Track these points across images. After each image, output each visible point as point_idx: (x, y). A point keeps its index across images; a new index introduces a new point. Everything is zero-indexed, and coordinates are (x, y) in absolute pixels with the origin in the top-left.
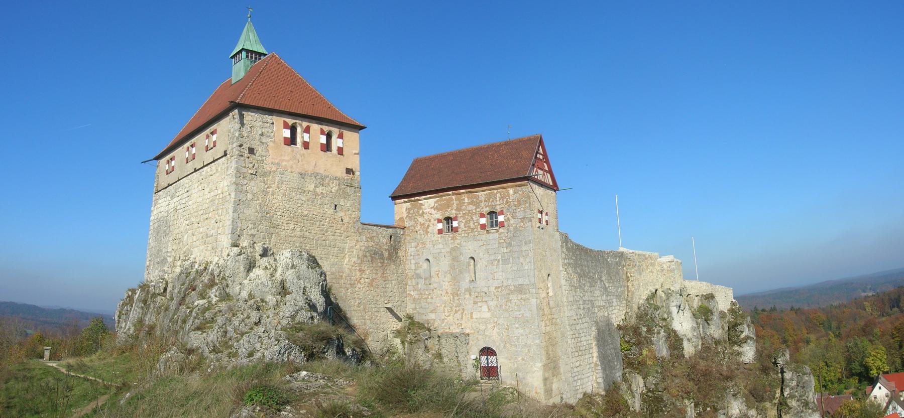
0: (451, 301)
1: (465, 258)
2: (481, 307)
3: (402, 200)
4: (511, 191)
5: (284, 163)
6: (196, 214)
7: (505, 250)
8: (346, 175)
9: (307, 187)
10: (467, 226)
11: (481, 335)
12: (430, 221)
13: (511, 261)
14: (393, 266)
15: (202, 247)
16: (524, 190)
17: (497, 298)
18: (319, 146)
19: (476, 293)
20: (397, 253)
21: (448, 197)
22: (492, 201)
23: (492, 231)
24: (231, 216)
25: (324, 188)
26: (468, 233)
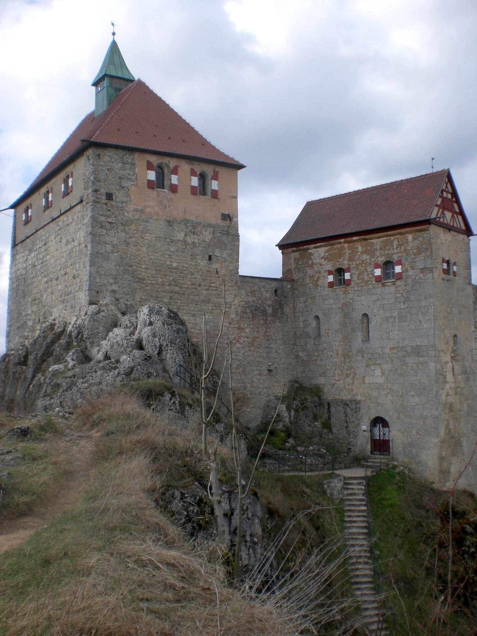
0: (341, 363)
1: (357, 315)
2: (374, 370)
3: (290, 250)
4: (410, 237)
5: (147, 210)
6: (54, 269)
7: (403, 307)
8: (221, 221)
9: (176, 236)
10: (360, 278)
11: (373, 403)
12: (320, 273)
13: (409, 318)
14: (278, 324)
15: (61, 306)
16: (425, 236)
17: (392, 360)
18: (189, 189)
19: (369, 355)
20: (282, 309)
21: (339, 246)
22: (389, 249)
23: (388, 284)
24: (88, 271)
25: (196, 236)
26: (362, 287)
